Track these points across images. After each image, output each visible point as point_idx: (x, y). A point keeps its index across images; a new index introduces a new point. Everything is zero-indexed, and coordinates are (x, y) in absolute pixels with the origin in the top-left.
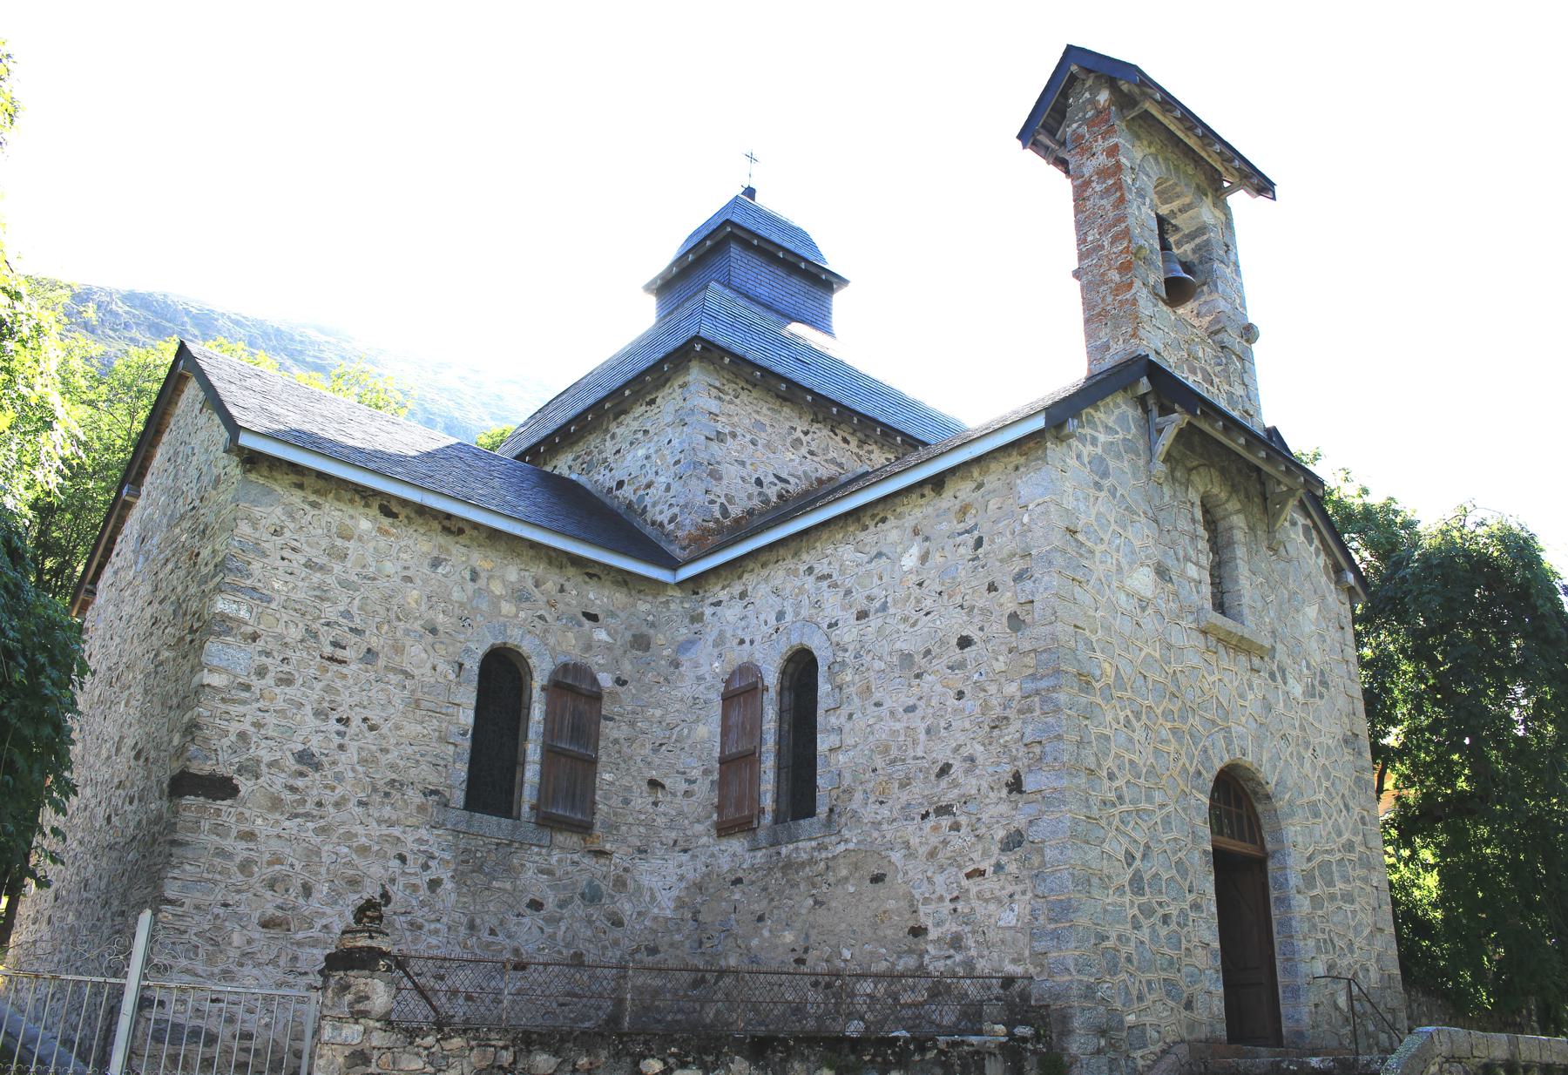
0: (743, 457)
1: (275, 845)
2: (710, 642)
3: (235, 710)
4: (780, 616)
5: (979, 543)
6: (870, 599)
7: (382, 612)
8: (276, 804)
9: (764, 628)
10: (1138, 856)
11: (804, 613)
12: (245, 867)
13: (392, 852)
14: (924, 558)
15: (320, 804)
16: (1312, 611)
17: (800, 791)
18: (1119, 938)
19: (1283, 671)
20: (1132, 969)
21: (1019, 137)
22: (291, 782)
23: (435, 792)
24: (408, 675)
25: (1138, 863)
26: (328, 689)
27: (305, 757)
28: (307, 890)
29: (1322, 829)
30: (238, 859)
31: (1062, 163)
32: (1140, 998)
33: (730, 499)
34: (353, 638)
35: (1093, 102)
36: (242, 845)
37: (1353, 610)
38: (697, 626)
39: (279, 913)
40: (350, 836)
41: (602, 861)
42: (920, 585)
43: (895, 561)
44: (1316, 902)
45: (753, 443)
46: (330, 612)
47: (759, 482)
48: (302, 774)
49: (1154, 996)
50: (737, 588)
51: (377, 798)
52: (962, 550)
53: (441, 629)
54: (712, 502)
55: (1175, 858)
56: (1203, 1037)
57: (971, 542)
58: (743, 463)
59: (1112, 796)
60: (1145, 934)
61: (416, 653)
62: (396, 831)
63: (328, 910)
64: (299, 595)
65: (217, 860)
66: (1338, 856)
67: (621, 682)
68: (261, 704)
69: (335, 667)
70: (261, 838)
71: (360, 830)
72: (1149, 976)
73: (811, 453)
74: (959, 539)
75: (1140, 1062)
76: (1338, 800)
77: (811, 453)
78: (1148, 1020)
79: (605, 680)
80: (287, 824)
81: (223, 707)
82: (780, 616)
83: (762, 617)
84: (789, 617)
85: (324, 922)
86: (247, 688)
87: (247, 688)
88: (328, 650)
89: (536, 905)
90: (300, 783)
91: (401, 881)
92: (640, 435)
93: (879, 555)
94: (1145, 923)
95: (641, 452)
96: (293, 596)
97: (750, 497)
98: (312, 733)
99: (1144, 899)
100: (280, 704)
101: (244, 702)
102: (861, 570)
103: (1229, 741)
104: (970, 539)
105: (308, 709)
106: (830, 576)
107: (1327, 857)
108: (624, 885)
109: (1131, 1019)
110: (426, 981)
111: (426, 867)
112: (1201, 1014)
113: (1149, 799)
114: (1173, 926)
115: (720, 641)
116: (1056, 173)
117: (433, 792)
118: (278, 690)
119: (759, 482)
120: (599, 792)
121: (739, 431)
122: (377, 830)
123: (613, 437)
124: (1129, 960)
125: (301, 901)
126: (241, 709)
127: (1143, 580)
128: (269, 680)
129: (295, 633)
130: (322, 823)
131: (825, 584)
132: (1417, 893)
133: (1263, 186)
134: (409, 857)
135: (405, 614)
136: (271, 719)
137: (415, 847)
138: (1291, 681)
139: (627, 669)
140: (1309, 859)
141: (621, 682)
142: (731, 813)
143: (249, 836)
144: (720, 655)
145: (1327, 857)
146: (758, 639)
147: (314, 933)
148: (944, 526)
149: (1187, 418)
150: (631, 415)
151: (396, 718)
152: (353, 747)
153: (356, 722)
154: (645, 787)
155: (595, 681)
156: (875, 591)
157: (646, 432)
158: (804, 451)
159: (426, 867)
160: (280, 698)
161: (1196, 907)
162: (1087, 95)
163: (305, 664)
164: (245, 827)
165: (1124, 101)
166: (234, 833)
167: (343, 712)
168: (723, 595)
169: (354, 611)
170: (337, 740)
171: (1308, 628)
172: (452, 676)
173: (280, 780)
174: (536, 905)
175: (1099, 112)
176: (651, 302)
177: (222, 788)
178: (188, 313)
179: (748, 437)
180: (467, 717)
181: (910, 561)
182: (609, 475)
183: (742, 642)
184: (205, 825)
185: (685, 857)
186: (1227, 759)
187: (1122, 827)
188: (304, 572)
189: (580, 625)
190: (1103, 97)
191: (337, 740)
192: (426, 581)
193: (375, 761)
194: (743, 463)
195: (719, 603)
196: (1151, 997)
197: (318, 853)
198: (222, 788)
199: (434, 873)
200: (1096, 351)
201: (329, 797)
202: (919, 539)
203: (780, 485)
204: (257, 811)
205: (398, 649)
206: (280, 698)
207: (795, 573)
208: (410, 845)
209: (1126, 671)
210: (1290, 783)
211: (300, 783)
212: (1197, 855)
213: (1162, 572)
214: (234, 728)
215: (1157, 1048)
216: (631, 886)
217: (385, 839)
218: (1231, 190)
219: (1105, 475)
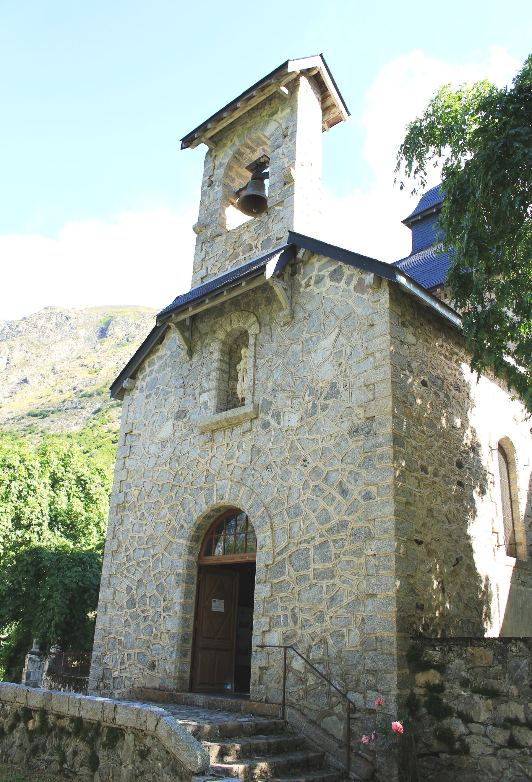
10: (134, 587)
18: (116, 633)
20: (121, 648)
29: (299, 525)
32: (122, 663)
37: (395, 473)
49: (131, 662)
56: (157, 686)
60: (131, 630)
72: (130, 651)
78: (124, 675)
109: (116, 674)
110: (158, 463)
124: (120, 643)
132: (436, 659)
161: (167, 609)
176: (408, 232)
187: (128, 575)
200: (200, 263)
212: (173, 578)
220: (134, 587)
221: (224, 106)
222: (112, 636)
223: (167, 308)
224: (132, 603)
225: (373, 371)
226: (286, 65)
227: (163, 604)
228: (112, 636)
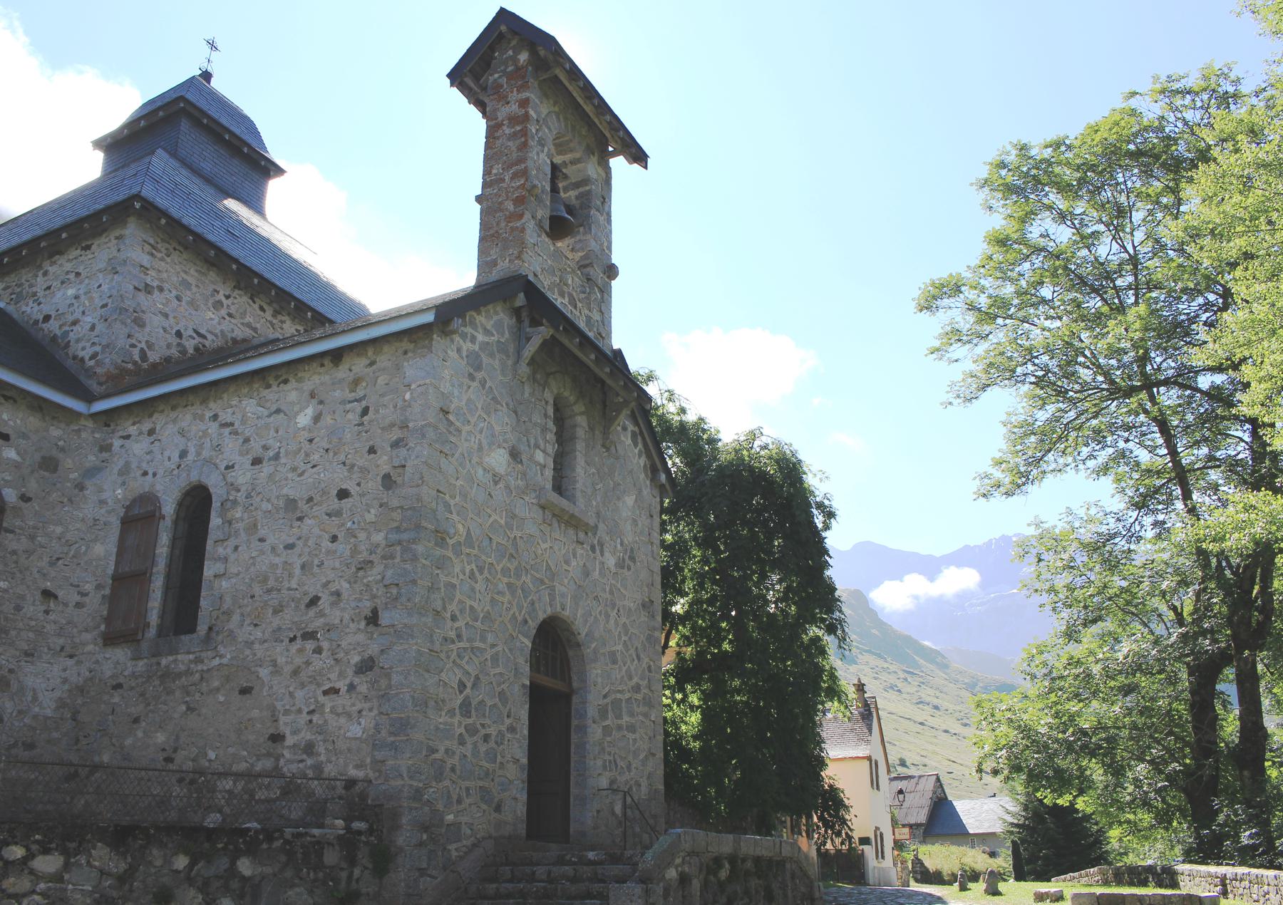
4: (183, 454)
5: (365, 411)
6: (265, 448)
14: (317, 418)
16: (630, 500)
19: (601, 545)
20: (454, 777)
25: (468, 691)
31: (480, 105)
32: (459, 801)
35: (514, 59)
38: (105, 455)
42: (311, 441)
45: (178, 298)
47: (179, 334)
50: (146, 426)
52: (350, 416)
54: (133, 346)
57: (359, 410)
58: (166, 316)
67: (25, 498)
73: (230, 315)
74: (348, 406)
77: (230, 315)
78: (464, 819)
82: (183, 454)
83: (167, 454)
84: (190, 457)
92: (72, 276)
93: (278, 411)
95: (71, 292)
104: (358, 407)
106: (232, 424)
107: (619, 696)
115: (126, 470)
121: (166, 286)
123: (45, 274)
124: (453, 770)
127: (498, 459)
131: (227, 431)
138: (607, 554)
139: (32, 486)
140: (605, 697)
141: (25, 498)
144: (124, 483)
145: (619, 696)
146: (161, 472)
148: (337, 393)
149: (551, 332)
156: (271, 442)
157: (78, 274)
158: (223, 312)
162: (511, 53)
168: (132, 430)
171: (625, 513)
181: (304, 419)
182: (36, 308)
183: (145, 473)
185: (70, 662)
187: (458, 661)
190: (523, 57)
194: (166, 316)
195: (128, 437)
202: (314, 401)
203: (198, 339)
212: (517, 688)
213: (514, 455)
215: (467, 842)
218: (614, 154)
220: (469, 685)
221: (616, 112)
222: (437, 756)
223: (344, 294)
224: (466, 708)
225: (60, 594)
226: (638, 156)
227: (508, 721)
228: (437, 756)
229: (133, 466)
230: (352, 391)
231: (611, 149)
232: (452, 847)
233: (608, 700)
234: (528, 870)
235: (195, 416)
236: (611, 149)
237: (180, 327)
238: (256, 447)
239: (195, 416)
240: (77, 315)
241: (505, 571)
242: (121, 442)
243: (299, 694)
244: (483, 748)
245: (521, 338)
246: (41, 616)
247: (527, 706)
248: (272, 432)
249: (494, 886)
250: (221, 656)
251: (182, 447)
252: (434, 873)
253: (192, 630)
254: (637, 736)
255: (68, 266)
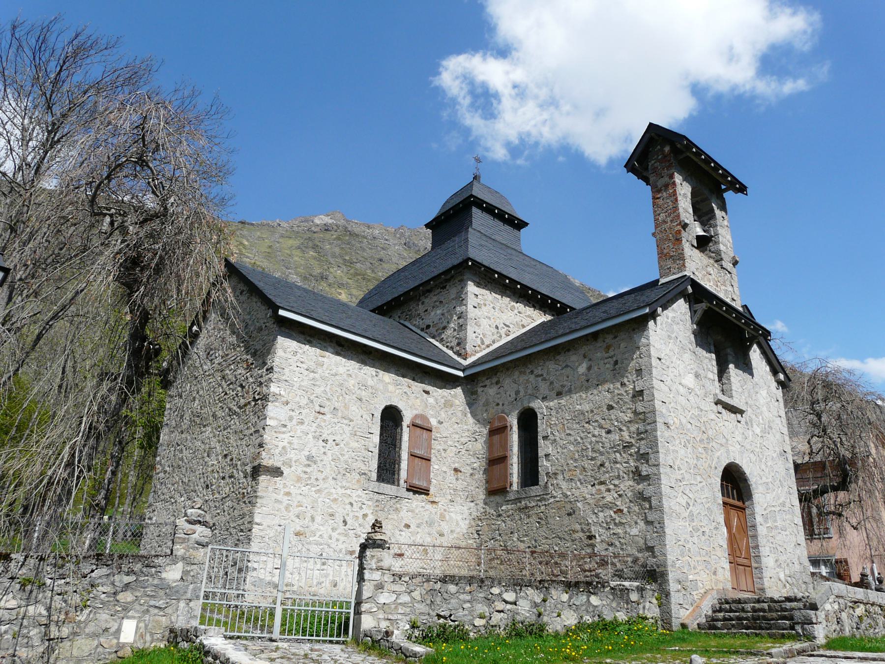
0: (489, 315)
1: (300, 498)
2: (481, 403)
3: (281, 436)
4: (517, 392)
5: (616, 363)
6: (563, 386)
7: (339, 391)
8: (299, 479)
9: (509, 399)
11: (529, 392)
12: (287, 508)
13: (347, 501)
14: (589, 368)
15: (317, 479)
16: (764, 393)
17: (531, 473)
19: (751, 421)
21: (625, 166)
22: (305, 469)
23: (365, 474)
24: (351, 421)
25: (691, 508)
26: (319, 426)
27: (310, 458)
28: (313, 519)
30: (285, 504)
31: (647, 181)
33: (484, 335)
34: (328, 403)
35: (662, 150)
36: (286, 498)
38: (474, 397)
39: (302, 529)
40: (330, 494)
41: (434, 506)
42: (588, 381)
43: (574, 369)
44: (770, 529)
45: (494, 308)
46: (318, 391)
47: (497, 327)
48: (309, 465)
50: (494, 380)
51: (339, 477)
52: (608, 366)
53: (364, 399)
54: (477, 337)
55: (706, 506)
57: (612, 362)
58: (489, 318)
59: (679, 477)
61: (355, 410)
62: (348, 492)
63: (321, 528)
64: (305, 383)
65: (276, 505)
66: (778, 508)
67: (440, 423)
68: (291, 434)
69: (321, 416)
70: (294, 495)
71: (333, 491)
73: (520, 313)
74: (606, 361)
75: (696, 597)
76: (778, 482)
77: (520, 313)
79: (433, 422)
80: (303, 488)
81: (276, 435)
82: (517, 392)
83: (508, 393)
84: (522, 394)
85: (320, 533)
86: (285, 426)
87: (285, 426)
88: (318, 409)
89: (408, 526)
90: (308, 470)
91: (351, 514)
92: (437, 303)
93: (567, 366)
94: (695, 534)
95: (439, 312)
96: (302, 384)
97: (493, 335)
98: (314, 447)
99: (694, 524)
100: (299, 433)
101: (284, 433)
102: (558, 373)
103: (728, 452)
104: (612, 361)
105: (310, 436)
106: (542, 375)
107: (773, 509)
108: (444, 517)
111: (361, 508)
112: (720, 576)
113: (695, 479)
114: (707, 537)
115: (487, 404)
116: (642, 183)
117: (365, 474)
118: (298, 427)
119: (497, 327)
120: (432, 474)
121: (487, 303)
122: (341, 491)
123: (423, 303)
125: (310, 523)
126: (283, 436)
127: (689, 380)
128: (294, 422)
129: (304, 401)
130: (318, 488)
131: (540, 379)
133: (742, 189)
134: (355, 504)
135: (348, 391)
136: (295, 441)
137: (357, 499)
138: (755, 426)
139: (443, 415)
140: (765, 510)
141: (440, 423)
142: (496, 485)
143: (288, 494)
144: (486, 410)
145: (773, 509)
146: (506, 403)
147: (316, 538)
148: (599, 354)
149: (709, 305)
150: (433, 293)
151: (346, 439)
152: (329, 453)
153: (331, 441)
154: (453, 472)
155: (429, 422)
156: (565, 383)
157: (441, 302)
158: (516, 311)
159: (361, 508)
160: (299, 431)
162: (659, 147)
163: (308, 414)
164: (287, 490)
165: (675, 151)
166: (282, 493)
167: (324, 436)
168: (488, 382)
169: (328, 390)
170: (323, 450)
171: (762, 401)
172: (369, 420)
173: (300, 469)
174: (408, 526)
175: (666, 156)
177: (277, 472)
178: (462, 327)
179: (492, 305)
180: (376, 439)
181: (582, 369)
182: (421, 322)
183: (498, 404)
184: (270, 489)
185: (472, 504)
186: (727, 462)
188: (306, 373)
189: (422, 396)
190: (667, 149)
191: (323, 450)
192: (356, 377)
193: (339, 459)
194: (489, 318)
195: (485, 386)
196: (699, 568)
197: (317, 501)
198: (277, 472)
199: (365, 511)
201: (321, 476)
202: (586, 360)
203: (506, 328)
204: (292, 483)
205: (346, 407)
206: (299, 431)
207: (524, 373)
208: (355, 498)
209: (684, 421)
210: (755, 474)
211: (308, 470)
213: (697, 376)
214: (281, 444)
215: (702, 591)
216: (447, 518)
217: (344, 495)
218: (726, 190)
219: (673, 332)
225: (462, 470)
229: (491, 400)
230: (607, 352)
231: (723, 187)
232: (694, 593)
233: (767, 512)
234: (740, 606)
235: (521, 373)
236: (723, 187)
237: (497, 323)
238: (557, 386)
239: (521, 373)
240: (445, 324)
241: (701, 441)
242: (482, 389)
243: (601, 514)
244: (703, 538)
245: (693, 312)
246: (454, 481)
247: (723, 516)
248: (565, 378)
249: (722, 614)
250: (555, 497)
251: (516, 389)
252: (687, 607)
253: (537, 484)
254: (788, 533)
255: (435, 299)
